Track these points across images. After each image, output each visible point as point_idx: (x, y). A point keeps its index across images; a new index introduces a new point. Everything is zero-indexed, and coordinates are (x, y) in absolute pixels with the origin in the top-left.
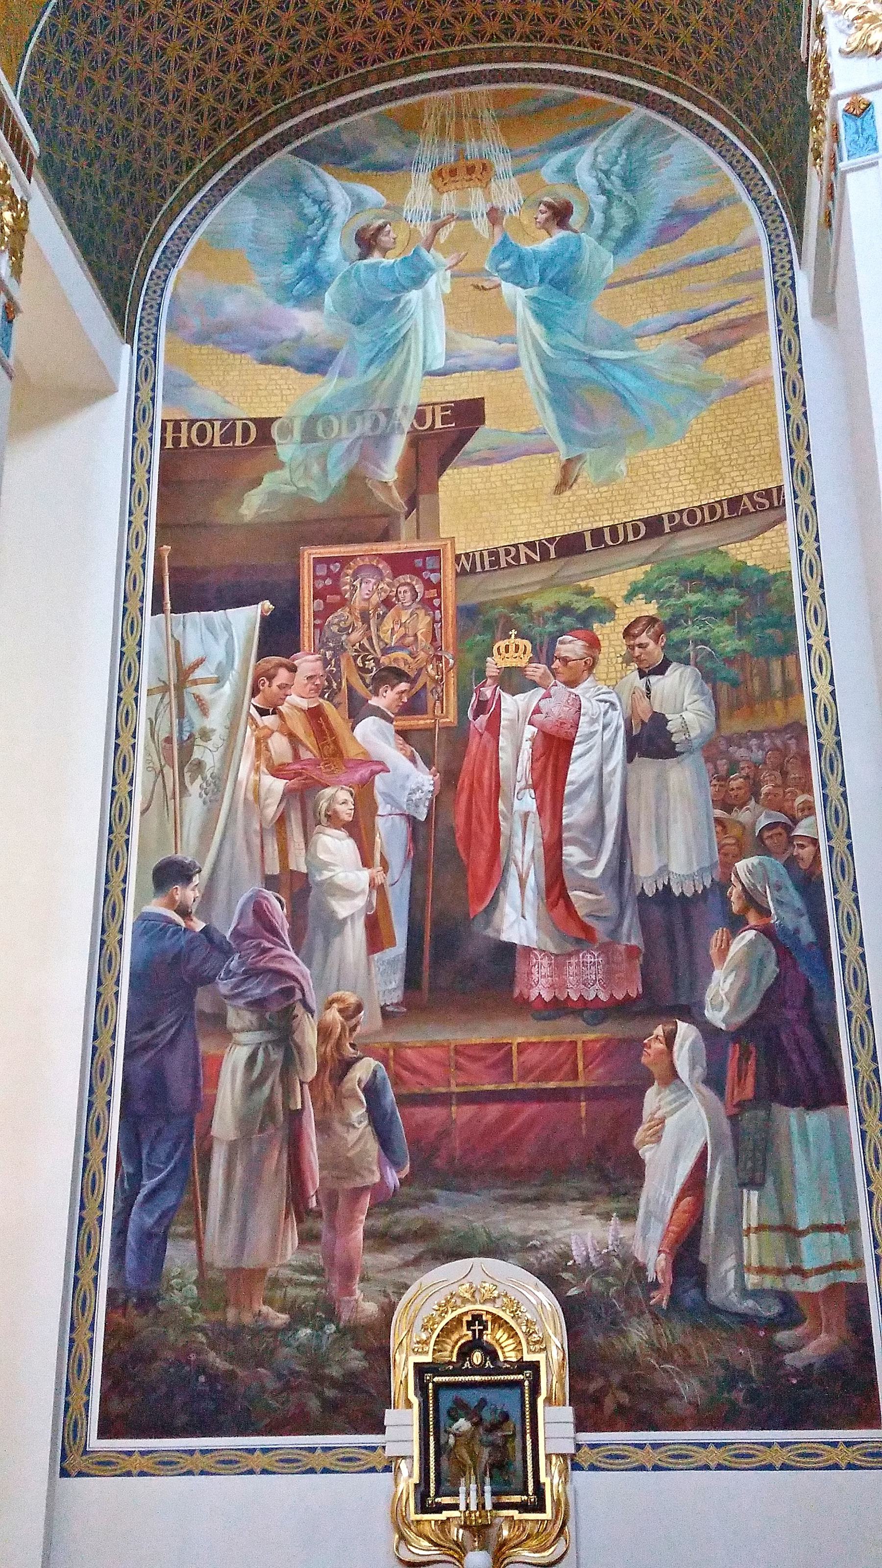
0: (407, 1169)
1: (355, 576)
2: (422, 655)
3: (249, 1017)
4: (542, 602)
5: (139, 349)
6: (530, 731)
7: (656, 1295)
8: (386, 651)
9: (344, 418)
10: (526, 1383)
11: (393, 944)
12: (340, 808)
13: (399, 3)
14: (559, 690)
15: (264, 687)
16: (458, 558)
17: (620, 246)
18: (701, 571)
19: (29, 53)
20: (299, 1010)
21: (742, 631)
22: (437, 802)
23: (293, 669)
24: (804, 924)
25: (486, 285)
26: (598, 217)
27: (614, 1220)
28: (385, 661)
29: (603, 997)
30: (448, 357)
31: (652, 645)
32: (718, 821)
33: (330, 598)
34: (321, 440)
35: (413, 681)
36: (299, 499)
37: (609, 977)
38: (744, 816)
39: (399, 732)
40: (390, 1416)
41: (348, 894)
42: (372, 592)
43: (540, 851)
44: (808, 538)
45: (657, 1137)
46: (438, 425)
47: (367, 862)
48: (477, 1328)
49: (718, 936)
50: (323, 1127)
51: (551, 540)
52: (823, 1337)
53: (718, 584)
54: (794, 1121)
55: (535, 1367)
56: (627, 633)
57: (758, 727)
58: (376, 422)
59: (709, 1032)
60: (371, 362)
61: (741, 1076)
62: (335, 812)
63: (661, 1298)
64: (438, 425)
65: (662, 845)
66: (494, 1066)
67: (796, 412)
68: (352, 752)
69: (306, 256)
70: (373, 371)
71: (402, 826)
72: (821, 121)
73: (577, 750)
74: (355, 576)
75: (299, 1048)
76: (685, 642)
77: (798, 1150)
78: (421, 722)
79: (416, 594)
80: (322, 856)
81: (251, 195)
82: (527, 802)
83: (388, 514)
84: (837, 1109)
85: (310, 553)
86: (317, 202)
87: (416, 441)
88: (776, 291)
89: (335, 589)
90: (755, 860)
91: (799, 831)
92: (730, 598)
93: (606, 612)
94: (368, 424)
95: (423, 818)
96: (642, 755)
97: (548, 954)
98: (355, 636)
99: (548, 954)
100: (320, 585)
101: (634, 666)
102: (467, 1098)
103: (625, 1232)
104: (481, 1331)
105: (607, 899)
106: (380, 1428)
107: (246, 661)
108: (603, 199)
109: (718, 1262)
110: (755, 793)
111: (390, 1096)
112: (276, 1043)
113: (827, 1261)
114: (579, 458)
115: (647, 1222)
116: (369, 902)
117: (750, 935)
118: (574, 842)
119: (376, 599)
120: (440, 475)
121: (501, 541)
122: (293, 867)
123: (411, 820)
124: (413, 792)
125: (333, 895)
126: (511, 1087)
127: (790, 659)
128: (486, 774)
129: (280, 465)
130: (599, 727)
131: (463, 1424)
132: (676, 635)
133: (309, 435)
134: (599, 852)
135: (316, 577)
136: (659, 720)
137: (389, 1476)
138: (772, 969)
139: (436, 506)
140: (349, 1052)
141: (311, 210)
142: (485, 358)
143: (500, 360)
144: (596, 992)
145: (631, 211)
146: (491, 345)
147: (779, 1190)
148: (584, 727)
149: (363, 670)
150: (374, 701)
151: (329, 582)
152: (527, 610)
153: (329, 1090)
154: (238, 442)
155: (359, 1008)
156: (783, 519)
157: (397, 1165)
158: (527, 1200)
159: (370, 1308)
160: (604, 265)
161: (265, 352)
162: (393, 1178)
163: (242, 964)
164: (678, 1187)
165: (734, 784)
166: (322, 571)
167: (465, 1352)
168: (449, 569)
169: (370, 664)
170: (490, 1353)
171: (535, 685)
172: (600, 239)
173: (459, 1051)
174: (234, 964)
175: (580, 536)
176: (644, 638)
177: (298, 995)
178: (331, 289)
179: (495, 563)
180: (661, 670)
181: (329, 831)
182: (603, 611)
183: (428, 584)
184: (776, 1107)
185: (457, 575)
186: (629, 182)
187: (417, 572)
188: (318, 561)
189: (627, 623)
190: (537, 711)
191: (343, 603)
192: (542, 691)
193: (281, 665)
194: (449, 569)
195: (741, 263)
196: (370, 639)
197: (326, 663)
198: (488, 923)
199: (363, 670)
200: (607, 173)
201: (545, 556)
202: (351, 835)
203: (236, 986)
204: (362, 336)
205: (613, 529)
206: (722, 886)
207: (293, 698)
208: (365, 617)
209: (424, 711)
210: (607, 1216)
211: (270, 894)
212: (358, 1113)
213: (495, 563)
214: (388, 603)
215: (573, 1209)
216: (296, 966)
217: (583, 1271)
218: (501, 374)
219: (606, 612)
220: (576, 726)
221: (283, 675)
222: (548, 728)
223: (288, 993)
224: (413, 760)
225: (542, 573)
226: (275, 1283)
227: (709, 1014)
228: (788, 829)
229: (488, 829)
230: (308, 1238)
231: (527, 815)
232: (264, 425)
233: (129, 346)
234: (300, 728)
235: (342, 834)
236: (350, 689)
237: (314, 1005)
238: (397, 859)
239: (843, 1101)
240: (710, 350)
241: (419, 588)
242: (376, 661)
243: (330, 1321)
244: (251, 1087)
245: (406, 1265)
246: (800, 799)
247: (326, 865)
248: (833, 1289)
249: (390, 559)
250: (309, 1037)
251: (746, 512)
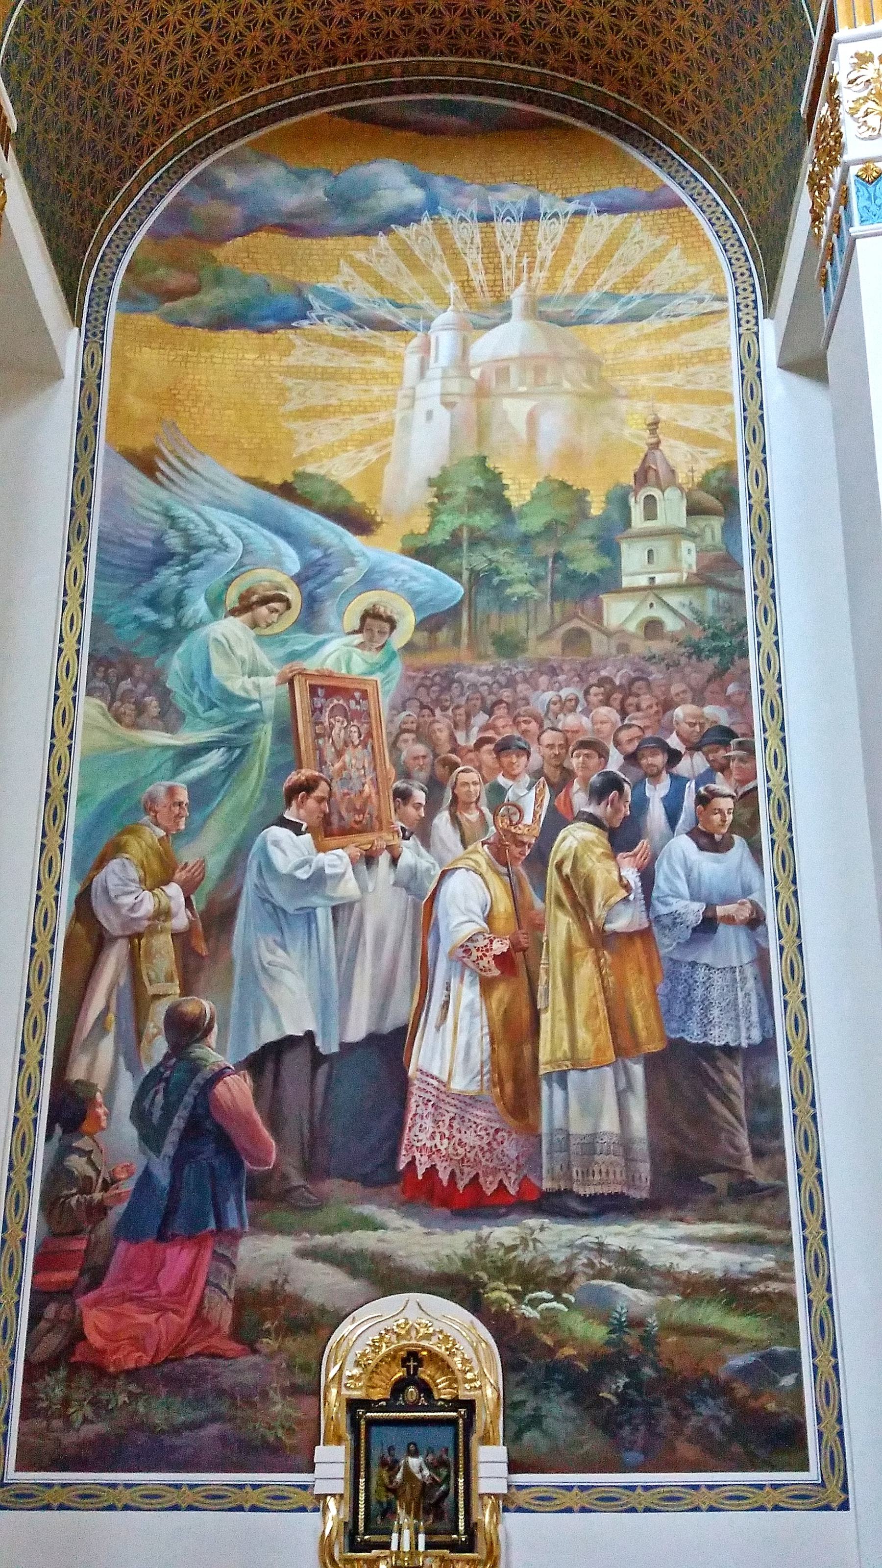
5: (87, 331)
10: (461, 1421)
13: (299, 3)
19: (14, 17)
40: (321, 1452)
48: (412, 1364)
55: (470, 1405)
72: (824, 186)
104: (416, 1369)
106: (311, 1469)
167: (399, 1388)
170: (425, 1389)
233: (77, 329)
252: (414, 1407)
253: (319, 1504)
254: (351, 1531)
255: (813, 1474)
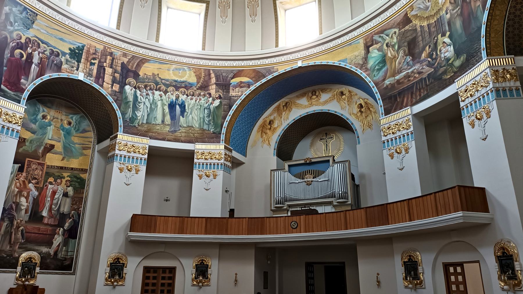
0: (25, 240)
1: (33, 164)
2: (40, 177)
3: (7, 219)
4: (57, 174)
6: (51, 190)
7: (51, 257)
8: (35, 175)
9: (36, 142)
11: (28, 213)
12: (25, 195)
14: (56, 186)
15: (18, 176)
16: (47, 165)
17: (76, 131)
18: (76, 176)
20: (14, 220)
21: (79, 185)
22: (38, 196)
23: (22, 175)
24: (78, 220)
25: (59, 130)
26: (74, 126)
27: (49, 248)
28: (35, 176)
29: (53, 224)
30: (51, 138)
31: (68, 183)
32: (71, 206)
33: (29, 166)
34: (32, 143)
35: (38, 180)
36: (27, 151)
37: (54, 222)
38: (74, 206)
39: (35, 186)
40: (18, 267)
41: (24, 206)
42: (35, 167)
43: (49, 205)
44: (89, 176)
45: (56, 240)
46: (48, 147)
47: (27, 202)
49: (68, 219)
50: (15, 234)
51: (59, 166)
52: (68, 262)
53: (78, 178)
54: (71, 240)
56: (66, 181)
57: (78, 196)
58: (40, 143)
59: (64, 229)
60: (41, 135)
61: (66, 235)
62: (24, 195)
63: (52, 257)
64: (48, 147)
65: (64, 207)
66: (38, 230)
67: (92, 161)
68: (28, 188)
69: (35, 116)
70: (41, 136)
71: (33, 199)
73: (57, 194)
74: (33, 164)
75: (13, 224)
76: (73, 184)
77: (70, 243)
78: (38, 186)
79: (40, 168)
80: (21, 200)
81: (29, 104)
82: (49, 199)
83: (39, 157)
84: (76, 240)
85: (27, 159)
86: (38, 109)
87: (45, 148)
88: (93, 145)
89: (30, 165)
90: (74, 212)
91: (80, 209)
92: (79, 180)
93: (64, 178)
94: (39, 144)
95: (35, 198)
96: (64, 196)
97: (47, 218)
98: (31, 172)
99: (47, 218)
100: (28, 164)
101: (66, 185)
102: (34, 233)
103: (49, 250)
105: (56, 213)
107: (16, 172)
108: (75, 124)
109: (59, 254)
110: (76, 204)
111: (24, 231)
112: (10, 223)
113: (71, 255)
114: (65, 157)
115: (52, 249)
116: (26, 208)
117: (71, 220)
118: (53, 205)
119: (35, 168)
120: (47, 153)
121: (53, 165)
122: (17, 201)
123: (34, 198)
124: (35, 194)
125: (22, 206)
126: (40, 232)
127: (84, 190)
128: (45, 194)
129: (26, 146)
130: (60, 192)
131: (26, 269)
132: (72, 183)
133: (30, 142)
134: (56, 207)
135: (27, 163)
136: (67, 193)
137: (16, 274)
138: (73, 224)
139: (46, 157)
140: (20, 226)
141: (37, 109)
142: (56, 140)
143: (58, 141)
144: (53, 223)
145: (78, 127)
146: (57, 138)
147: (67, 247)
148: (58, 191)
149: (31, 177)
150: (32, 181)
151: (29, 164)
152: (55, 175)
153: (16, 230)
154: (21, 141)
155: (22, 220)
156: (87, 173)
157: (24, 240)
158: (39, 245)
159: (17, 255)
160: (74, 133)
161: (27, 129)
162: (23, 241)
163: (8, 212)
164: (57, 245)
165: (74, 202)
166: (29, 162)
168: (45, 167)
169: (33, 176)
170: (204, 263)
171: (53, 184)
172: (74, 129)
173: (34, 227)
174: (7, 212)
175: (63, 167)
176: (68, 182)
177: (15, 218)
178: (38, 122)
179: (52, 167)
180: (69, 187)
181: (23, 197)
182: (64, 177)
183: (42, 168)
184: (70, 239)
185: (46, 167)
186: (79, 123)
187: (41, 166)
188: (28, 160)
189: (66, 180)
190: (53, 188)
191: (31, 167)
192: (54, 186)
193: (21, 174)
194: (45, 167)
195: (90, 140)
196: (33, 173)
197: (27, 175)
198: (41, 213)
199: (31, 177)
200: (77, 120)
201: (58, 168)
202: (25, 198)
203: (7, 215)
204: (41, 131)
205: (67, 167)
206: (69, 214)
207: (21, 178)
208: (33, 170)
209: (38, 184)
210: (48, 248)
211: (13, 204)
212: (20, 233)
213: (52, 167)
214: (36, 169)
215: (44, 247)
216: (15, 214)
217: (43, 253)
218: (58, 143)
219: (64, 178)
220: (57, 191)
221: (20, 175)
222: (54, 190)
223: (14, 217)
224: (36, 190)
225: (57, 170)
226: (6, 252)
227: (65, 228)
228: (79, 209)
229: (44, 201)
230: (10, 247)
231: (49, 200)
232: (25, 139)
234: (21, 183)
235: (25, 198)
236: (29, 179)
237: (16, 219)
238: (31, 203)
239: (77, 239)
240: (84, 149)
241: (41, 168)
242: (33, 176)
243: (11, 256)
244: (6, 228)
245: (22, 251)
246: (81, 206)
247: (21, 202)
248: (70, 257)
249: (38, 163)
250: (15, 223)
251: (83, 171)
252: (202, 265)
253: (16, 273)
254: (195, 277)
255: (72, 272)
